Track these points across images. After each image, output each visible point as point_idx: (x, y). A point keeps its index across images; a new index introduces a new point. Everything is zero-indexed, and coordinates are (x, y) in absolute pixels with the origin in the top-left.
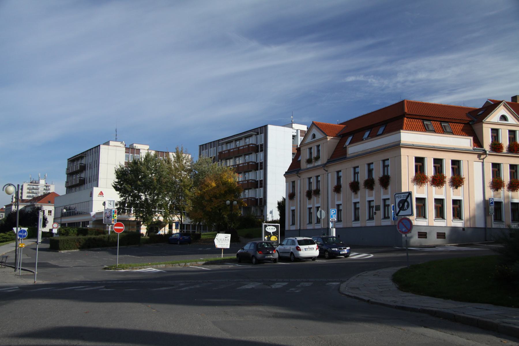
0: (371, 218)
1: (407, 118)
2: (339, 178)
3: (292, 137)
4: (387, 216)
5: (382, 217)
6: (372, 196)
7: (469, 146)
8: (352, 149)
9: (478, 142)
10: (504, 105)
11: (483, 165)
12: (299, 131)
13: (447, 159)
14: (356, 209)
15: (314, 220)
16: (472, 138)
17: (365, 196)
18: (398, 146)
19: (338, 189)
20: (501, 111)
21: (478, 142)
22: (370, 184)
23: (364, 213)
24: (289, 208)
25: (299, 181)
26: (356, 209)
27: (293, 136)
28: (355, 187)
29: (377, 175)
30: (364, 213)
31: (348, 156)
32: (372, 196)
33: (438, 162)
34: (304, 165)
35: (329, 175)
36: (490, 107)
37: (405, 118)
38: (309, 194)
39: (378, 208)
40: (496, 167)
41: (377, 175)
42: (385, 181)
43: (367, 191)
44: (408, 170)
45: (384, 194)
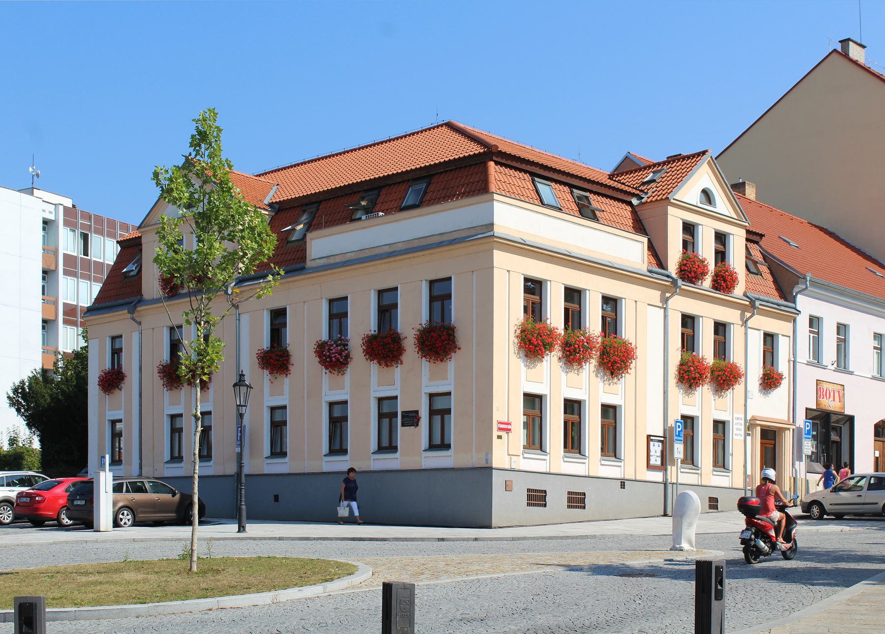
0: (387, 446)
1: (497, 163)
2: (116, 352)
3: (41, 225)
4: (177, 455)
5: (424, 442)
6: (445, 378)
7: (640, 261)
8: (323, 244)
9: (657, 254)
10: (709, 163)
11: (665, 316)
12: (61, 209)
13: (595, 288)
14: (176, 432)
15: (500, 433)
16: (645, 240)
17: (365, 385)
18: (483, 236)
19: (276, 359)
20: (703, 177)
21: (657, 254)
22: (385, 348)
23: (363, 429)
24: (102, 415)
25: (135, 336)
26: (176, 432)
27: (46, 222)
28: (333, 356)
29: (412, 317)
30: (363, 429)
31: (309, 264)
32: (445, 378)
33: (573, 295)
34: (151, 286)
35: (245, 319)
36: (681, 163)
37: (492, 164)
38: (171, 375)
39: (411, 418)
40: (688, 321)
41: (412, 317)
42: (439, 341)
43: (374, 366)
44: (508, 312)
45: (172, 404)
